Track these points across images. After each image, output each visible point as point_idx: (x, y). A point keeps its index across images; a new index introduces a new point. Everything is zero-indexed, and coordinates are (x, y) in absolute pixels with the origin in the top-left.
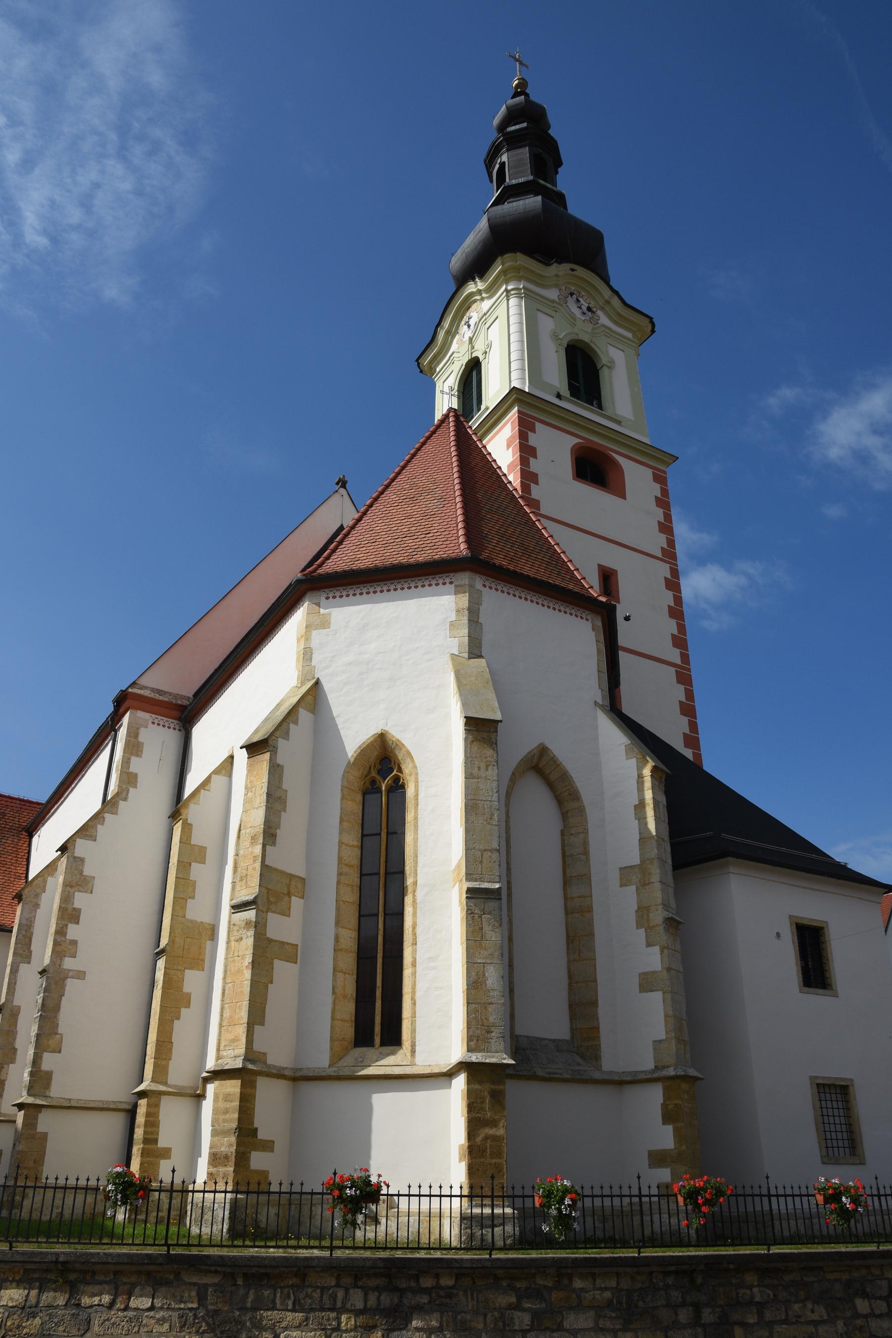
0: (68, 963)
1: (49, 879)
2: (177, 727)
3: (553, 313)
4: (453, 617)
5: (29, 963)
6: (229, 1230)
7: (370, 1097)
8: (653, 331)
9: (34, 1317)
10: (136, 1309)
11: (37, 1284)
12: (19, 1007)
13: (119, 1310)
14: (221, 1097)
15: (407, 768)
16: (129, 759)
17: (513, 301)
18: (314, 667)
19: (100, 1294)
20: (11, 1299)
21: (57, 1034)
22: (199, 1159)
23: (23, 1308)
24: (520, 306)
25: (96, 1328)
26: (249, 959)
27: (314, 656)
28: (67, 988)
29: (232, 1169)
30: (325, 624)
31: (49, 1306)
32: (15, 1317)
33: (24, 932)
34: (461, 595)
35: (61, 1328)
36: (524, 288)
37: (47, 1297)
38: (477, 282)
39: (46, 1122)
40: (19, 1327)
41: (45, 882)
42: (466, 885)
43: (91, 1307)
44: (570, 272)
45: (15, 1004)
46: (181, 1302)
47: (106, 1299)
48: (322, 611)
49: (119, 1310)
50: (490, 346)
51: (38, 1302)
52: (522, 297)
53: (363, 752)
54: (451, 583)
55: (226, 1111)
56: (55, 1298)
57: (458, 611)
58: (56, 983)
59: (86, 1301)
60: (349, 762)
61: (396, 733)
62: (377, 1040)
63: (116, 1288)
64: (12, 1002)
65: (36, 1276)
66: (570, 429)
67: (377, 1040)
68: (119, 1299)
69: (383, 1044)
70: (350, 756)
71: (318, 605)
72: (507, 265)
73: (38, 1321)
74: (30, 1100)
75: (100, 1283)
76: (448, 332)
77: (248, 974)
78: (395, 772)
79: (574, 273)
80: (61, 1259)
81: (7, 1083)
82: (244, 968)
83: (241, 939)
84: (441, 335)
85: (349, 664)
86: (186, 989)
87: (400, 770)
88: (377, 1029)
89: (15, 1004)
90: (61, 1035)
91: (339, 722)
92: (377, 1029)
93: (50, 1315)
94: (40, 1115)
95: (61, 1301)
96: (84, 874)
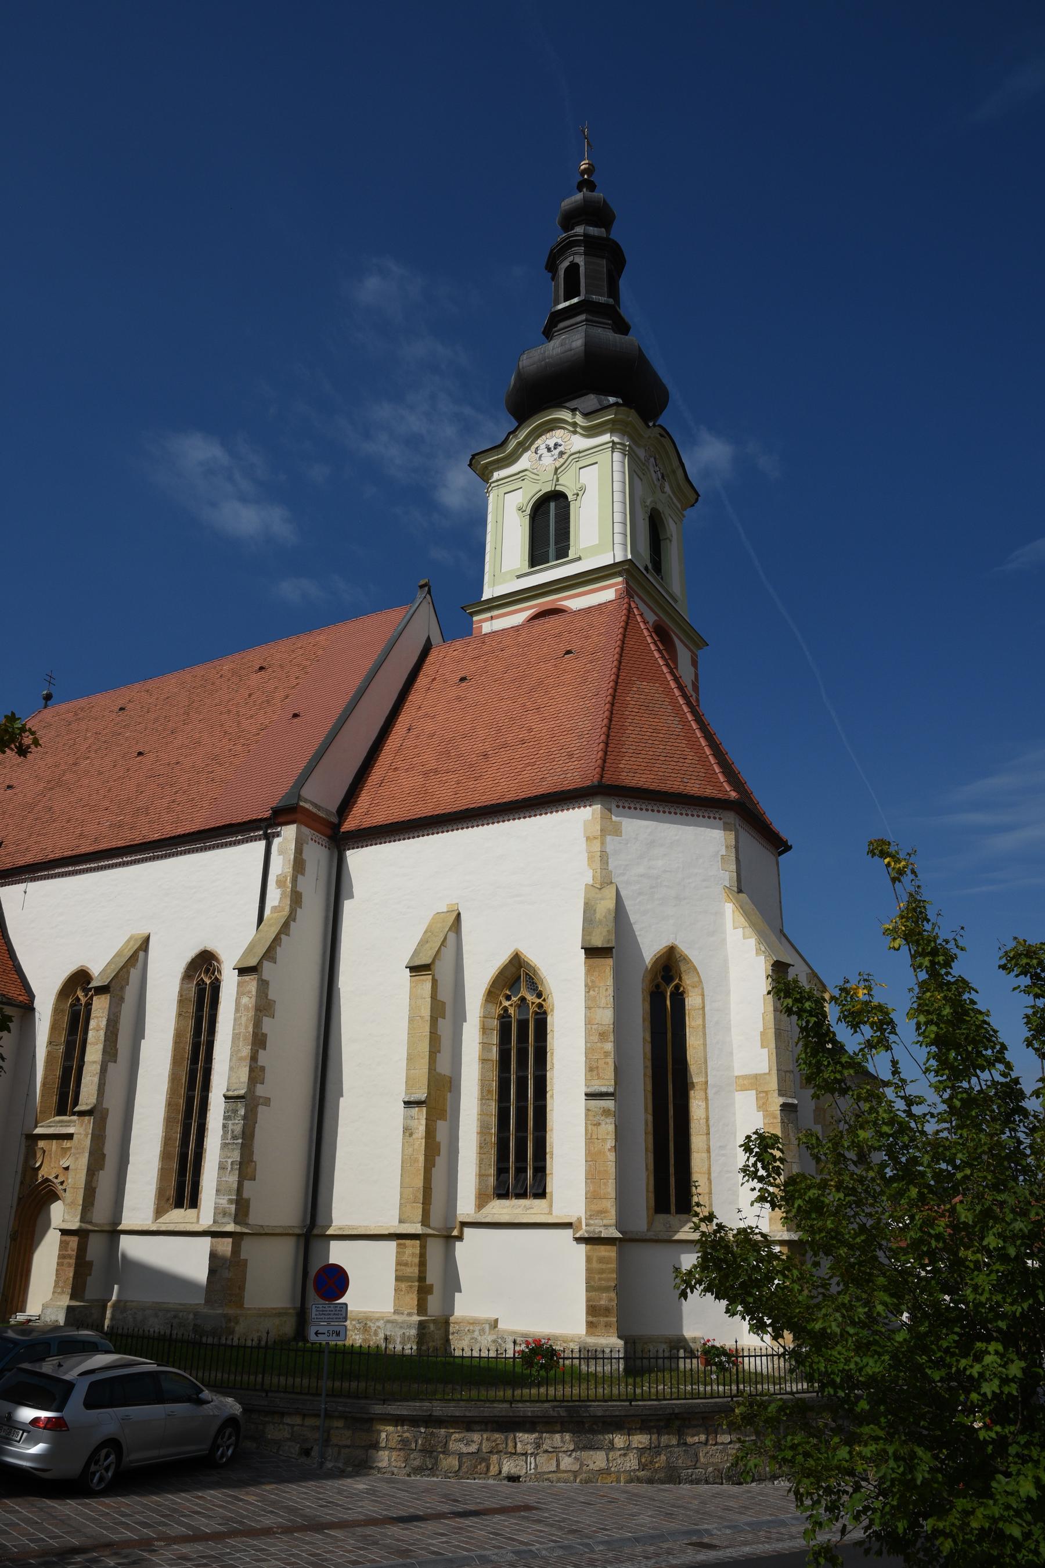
0: (260, 1090)
1: (132, 970)
2: (324, 843)
3: (642, 476)
4: (723, 852)
5: (115, 1062)
6: (625, 1369)
7: (679, 1257)
8: (693, 505)
9: (660, 1455)
10: (722, 1443)
11: (655, 1430)
12: (108, 1110)
13: (712, 1445)
14: (595, 1259)
15: (688, 981)
16: (297, 877)
17: (617, 456)
18: (611, 872)
19: (697, 1434)
20: (640, 1443)
21: (252, 1161)
22: (457, 1294)
23: (650, 1449)
24: (623, 463)
25: (702, 1460)
26: (611, 1143)
27: (610, 861)
28: (259, 1115)
29: (615, 1319)
30: (617, 831)
31: (668, 1446)
32: (646, 1455)
33: (111, 1028)
34: (728, 832)
35: (680, 1461)
36: (629, 446)
37: (665, 1439)
38: (576, 414)
39: (250, 1250)
40: (651, 1462)
41: (128, 973)
42: (781, 1100)
43: (694, 1444)
44: (658, 436)
45: (104, 1106)
46: (746, 1436)
47: (703, 1437)
48: (614, 818)
49: (712, 1445)
50: (583, 489)
51: (659, 1443)
52: (625, 455)
53: (656, 962)
54: (720, 819)
55: (602, 1271)
56: (669, 1439)
57: (727, 847)
58: (251, 1111)
59: (690, 1440)
60: (647, 968)
61: (684, 948)
62: (673, 1208)
63: (707, 1429)
64: (102, 1105)
65: (652, 1424)
66: (642, 595)
67: (673, 1208)
68: (710, 1437)
69: (678, 1212)
70: (647, 962)
71: (610, 810)
72: (619, 417)
73: (663, 1457)
74: (238, 1229)
75: (695, 1426)
76: (520, 444)
77: (611, 1156)
78: (677, 981)
79: (662, 439)
80: (677, 1411)
81: (97, 1190)
82: (606, 1150)
83: (600, 1124)
84: (512, 444)
85: (641, 876)
86: (438, 1139)
87: (680, 979)
88: (673, 1199)
89: (104, 1106)
90: (255, 1162)
91: (636, 927)
92: (673, 1199)
93: (670, 1452)
94: (243, 1242)
95: (674, 1442)
96: (269, 997)
